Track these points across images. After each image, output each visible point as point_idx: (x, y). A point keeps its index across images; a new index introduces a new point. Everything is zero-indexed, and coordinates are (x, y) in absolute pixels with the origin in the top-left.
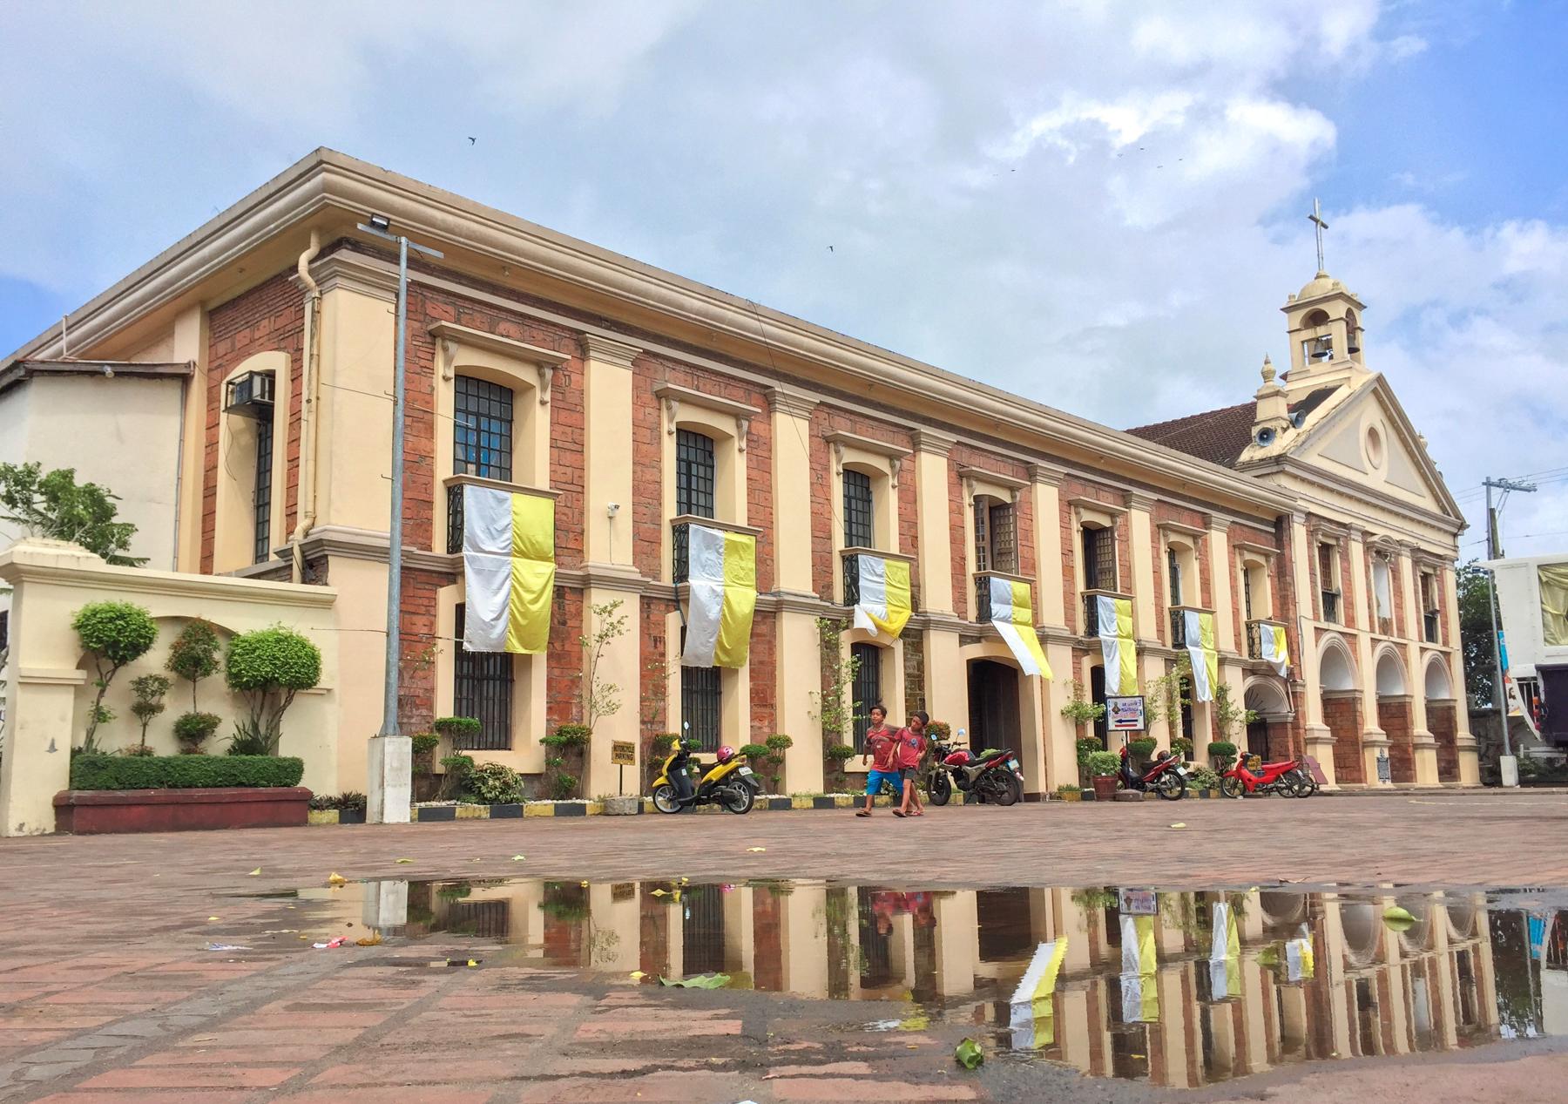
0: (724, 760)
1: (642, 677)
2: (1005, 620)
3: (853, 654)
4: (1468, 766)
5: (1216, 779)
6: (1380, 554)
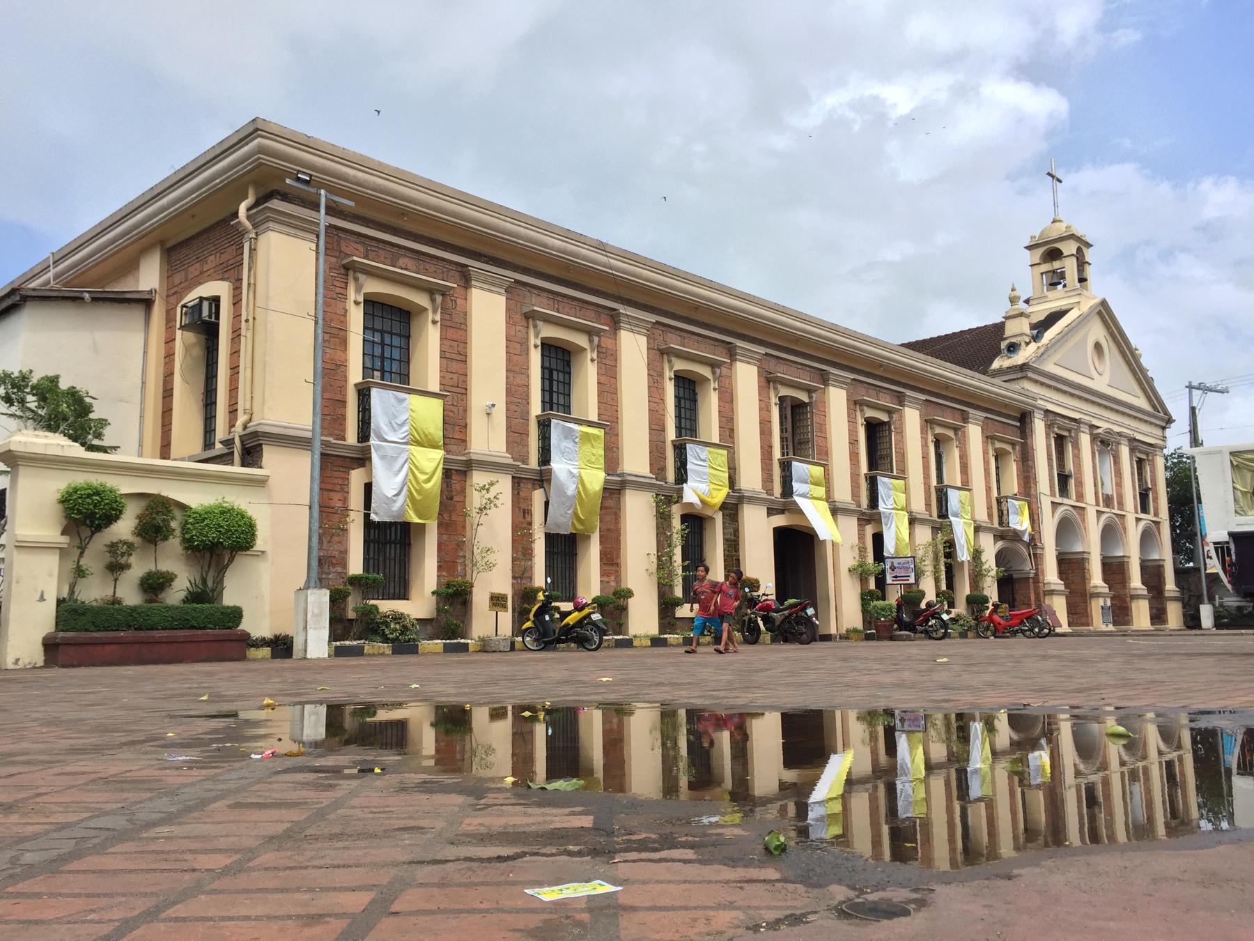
0: (579, 608)
1: (514, 541)
2: (803, 496)
4: (1174, 613)
5: (973, 623)
6: (1104, 443)
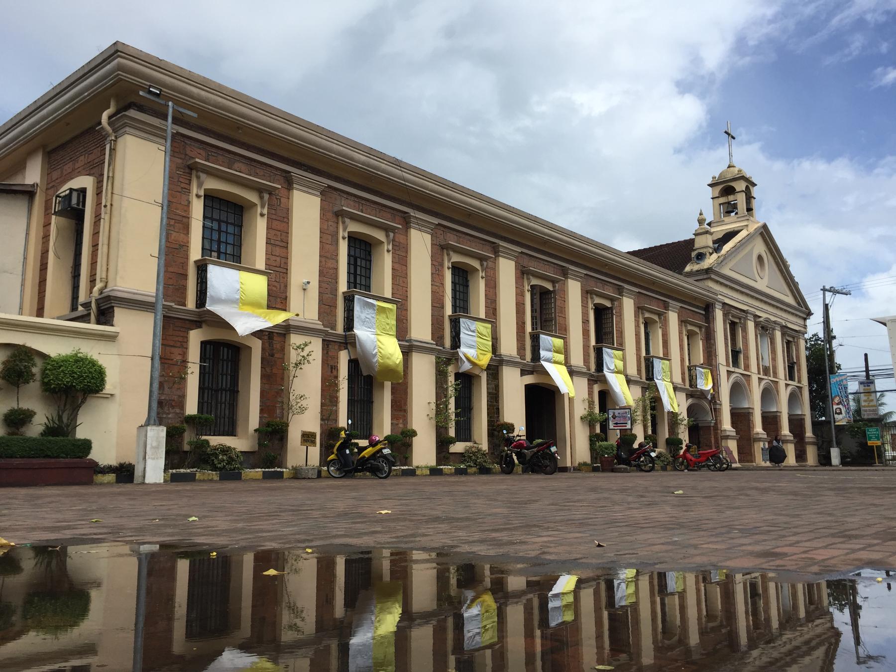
0: (373, 444)
4: (811, 453)
5: (671, 459)
6: (764, 328)
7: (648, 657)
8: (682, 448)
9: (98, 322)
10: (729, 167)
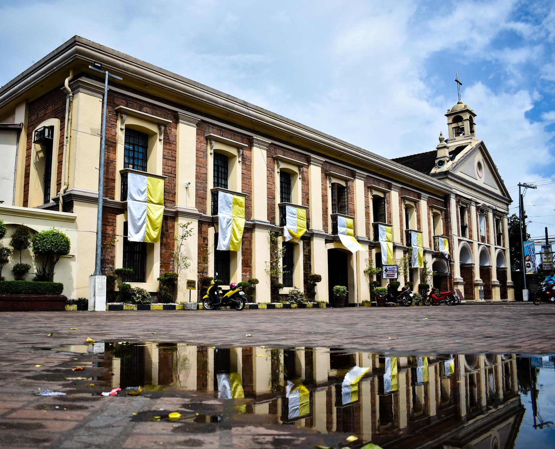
0: (233, 288)
1: (199, 253)
2: (343, 233)
3: (283, 246)
4: (511, 293)
5: (421, 298)
6: (482, 211)
7: (403, 423)
8: (429, 291)
9: (64, 210)
10: (458, 103)
